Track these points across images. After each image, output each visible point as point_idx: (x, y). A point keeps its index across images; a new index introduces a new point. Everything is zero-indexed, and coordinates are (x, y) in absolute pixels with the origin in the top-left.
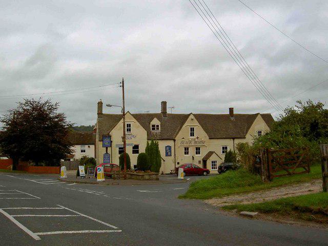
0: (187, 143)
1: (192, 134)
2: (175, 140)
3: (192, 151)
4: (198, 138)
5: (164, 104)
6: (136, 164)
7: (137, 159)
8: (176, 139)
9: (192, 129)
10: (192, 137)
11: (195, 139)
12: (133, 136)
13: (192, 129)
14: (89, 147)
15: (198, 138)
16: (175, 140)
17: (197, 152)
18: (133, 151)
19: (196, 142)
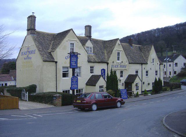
1: (118, 59)
2: (108, 64)
4: (122, 62)
9: (118, 54)
10: (118, 61)
13: (118, 54)
16: (108, 64)
19: (121, 66)
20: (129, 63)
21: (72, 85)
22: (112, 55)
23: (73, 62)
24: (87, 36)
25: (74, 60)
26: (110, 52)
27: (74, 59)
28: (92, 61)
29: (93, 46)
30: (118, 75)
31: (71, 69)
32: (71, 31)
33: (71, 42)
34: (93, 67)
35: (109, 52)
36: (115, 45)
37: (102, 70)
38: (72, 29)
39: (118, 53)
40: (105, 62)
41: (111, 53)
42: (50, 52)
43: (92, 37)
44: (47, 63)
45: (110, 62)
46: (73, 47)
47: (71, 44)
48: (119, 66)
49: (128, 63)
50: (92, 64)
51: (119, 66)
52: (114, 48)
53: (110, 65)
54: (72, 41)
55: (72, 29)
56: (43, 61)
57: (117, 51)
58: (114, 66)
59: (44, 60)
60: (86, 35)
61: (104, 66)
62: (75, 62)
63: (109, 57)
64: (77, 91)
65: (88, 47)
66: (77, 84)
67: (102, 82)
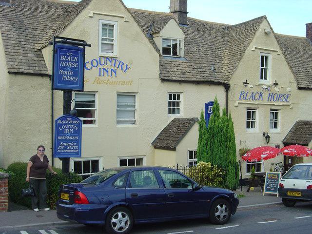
0: (253, 97)
1: (263, 75)
2: (227, 87)
3: (261, 118)
4: (276, 84)
5: (90, 46)
6: (285, 186)
7: (257, 147)
8: (231, 83)
9: (264, 60)
10: (263, 81)
11: (269, 88)
12: (121, 64)
13: (264, 60)
14: (294, 185)
15: (276, 84)
16: (227, 87)
17: (170, 110)
18: (93, 106)
19: (271, 96)
20: (300, 88)
21: (59, 144)
22: (241, 63)
23: (65, 69)
24: (175, 12)
25: (69, 64)
26: (238, 55)
27: (69, 61)
28: (174, 78)
29: (183, 36)
30: (239, 119)
31: (61, 93)
32: (265, 22)
33: (105, 22)
34: (179, 96)
35: (235, 55)
36: (254, 34)
37: (207, 105)
38: (265, 17)
39: (262, 57)
40: (219, 84)
41: (240, 58)
42: (40, 50)
43: (188, 15)
44: (20, 78)
45: (236, 82)
46: (112, 34)
47: (105, 25)
48: (266, 96)
49: (296, 86)
50: (175, 88)
51: (266, 96)
52: (249, 43)
53: (235, 92)
54: (265, 52)
55: (265, 17)
56: (10, 73)
57: (259, 51)
58: (249, 95)
59: (12, 70)
60: (173, 10)
61: (216, 94)
62: (73, 69)
63: (234, 68)
64: (77, 164)
65: (107, 25)
66: (79, 143)
67: (192, 140)
